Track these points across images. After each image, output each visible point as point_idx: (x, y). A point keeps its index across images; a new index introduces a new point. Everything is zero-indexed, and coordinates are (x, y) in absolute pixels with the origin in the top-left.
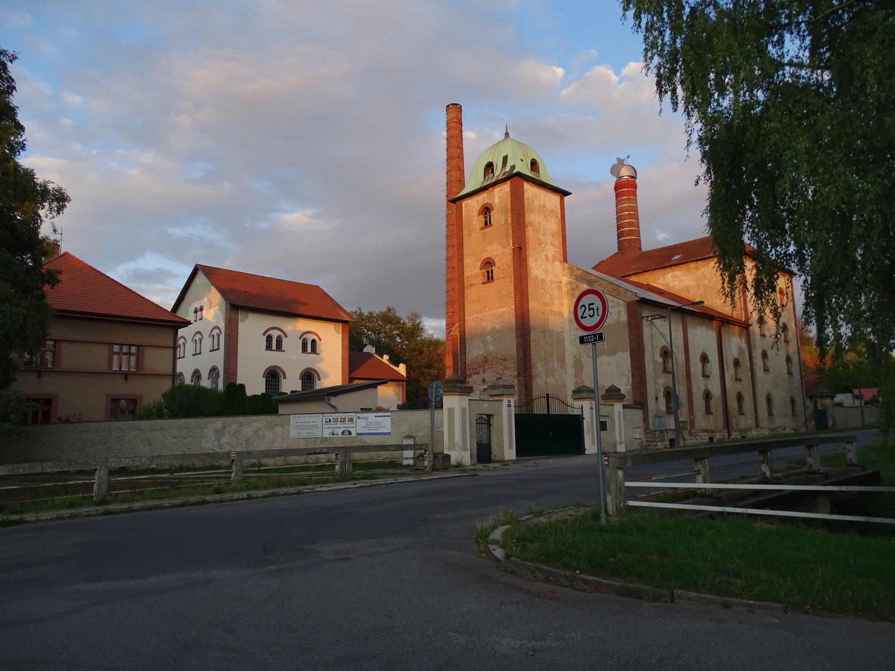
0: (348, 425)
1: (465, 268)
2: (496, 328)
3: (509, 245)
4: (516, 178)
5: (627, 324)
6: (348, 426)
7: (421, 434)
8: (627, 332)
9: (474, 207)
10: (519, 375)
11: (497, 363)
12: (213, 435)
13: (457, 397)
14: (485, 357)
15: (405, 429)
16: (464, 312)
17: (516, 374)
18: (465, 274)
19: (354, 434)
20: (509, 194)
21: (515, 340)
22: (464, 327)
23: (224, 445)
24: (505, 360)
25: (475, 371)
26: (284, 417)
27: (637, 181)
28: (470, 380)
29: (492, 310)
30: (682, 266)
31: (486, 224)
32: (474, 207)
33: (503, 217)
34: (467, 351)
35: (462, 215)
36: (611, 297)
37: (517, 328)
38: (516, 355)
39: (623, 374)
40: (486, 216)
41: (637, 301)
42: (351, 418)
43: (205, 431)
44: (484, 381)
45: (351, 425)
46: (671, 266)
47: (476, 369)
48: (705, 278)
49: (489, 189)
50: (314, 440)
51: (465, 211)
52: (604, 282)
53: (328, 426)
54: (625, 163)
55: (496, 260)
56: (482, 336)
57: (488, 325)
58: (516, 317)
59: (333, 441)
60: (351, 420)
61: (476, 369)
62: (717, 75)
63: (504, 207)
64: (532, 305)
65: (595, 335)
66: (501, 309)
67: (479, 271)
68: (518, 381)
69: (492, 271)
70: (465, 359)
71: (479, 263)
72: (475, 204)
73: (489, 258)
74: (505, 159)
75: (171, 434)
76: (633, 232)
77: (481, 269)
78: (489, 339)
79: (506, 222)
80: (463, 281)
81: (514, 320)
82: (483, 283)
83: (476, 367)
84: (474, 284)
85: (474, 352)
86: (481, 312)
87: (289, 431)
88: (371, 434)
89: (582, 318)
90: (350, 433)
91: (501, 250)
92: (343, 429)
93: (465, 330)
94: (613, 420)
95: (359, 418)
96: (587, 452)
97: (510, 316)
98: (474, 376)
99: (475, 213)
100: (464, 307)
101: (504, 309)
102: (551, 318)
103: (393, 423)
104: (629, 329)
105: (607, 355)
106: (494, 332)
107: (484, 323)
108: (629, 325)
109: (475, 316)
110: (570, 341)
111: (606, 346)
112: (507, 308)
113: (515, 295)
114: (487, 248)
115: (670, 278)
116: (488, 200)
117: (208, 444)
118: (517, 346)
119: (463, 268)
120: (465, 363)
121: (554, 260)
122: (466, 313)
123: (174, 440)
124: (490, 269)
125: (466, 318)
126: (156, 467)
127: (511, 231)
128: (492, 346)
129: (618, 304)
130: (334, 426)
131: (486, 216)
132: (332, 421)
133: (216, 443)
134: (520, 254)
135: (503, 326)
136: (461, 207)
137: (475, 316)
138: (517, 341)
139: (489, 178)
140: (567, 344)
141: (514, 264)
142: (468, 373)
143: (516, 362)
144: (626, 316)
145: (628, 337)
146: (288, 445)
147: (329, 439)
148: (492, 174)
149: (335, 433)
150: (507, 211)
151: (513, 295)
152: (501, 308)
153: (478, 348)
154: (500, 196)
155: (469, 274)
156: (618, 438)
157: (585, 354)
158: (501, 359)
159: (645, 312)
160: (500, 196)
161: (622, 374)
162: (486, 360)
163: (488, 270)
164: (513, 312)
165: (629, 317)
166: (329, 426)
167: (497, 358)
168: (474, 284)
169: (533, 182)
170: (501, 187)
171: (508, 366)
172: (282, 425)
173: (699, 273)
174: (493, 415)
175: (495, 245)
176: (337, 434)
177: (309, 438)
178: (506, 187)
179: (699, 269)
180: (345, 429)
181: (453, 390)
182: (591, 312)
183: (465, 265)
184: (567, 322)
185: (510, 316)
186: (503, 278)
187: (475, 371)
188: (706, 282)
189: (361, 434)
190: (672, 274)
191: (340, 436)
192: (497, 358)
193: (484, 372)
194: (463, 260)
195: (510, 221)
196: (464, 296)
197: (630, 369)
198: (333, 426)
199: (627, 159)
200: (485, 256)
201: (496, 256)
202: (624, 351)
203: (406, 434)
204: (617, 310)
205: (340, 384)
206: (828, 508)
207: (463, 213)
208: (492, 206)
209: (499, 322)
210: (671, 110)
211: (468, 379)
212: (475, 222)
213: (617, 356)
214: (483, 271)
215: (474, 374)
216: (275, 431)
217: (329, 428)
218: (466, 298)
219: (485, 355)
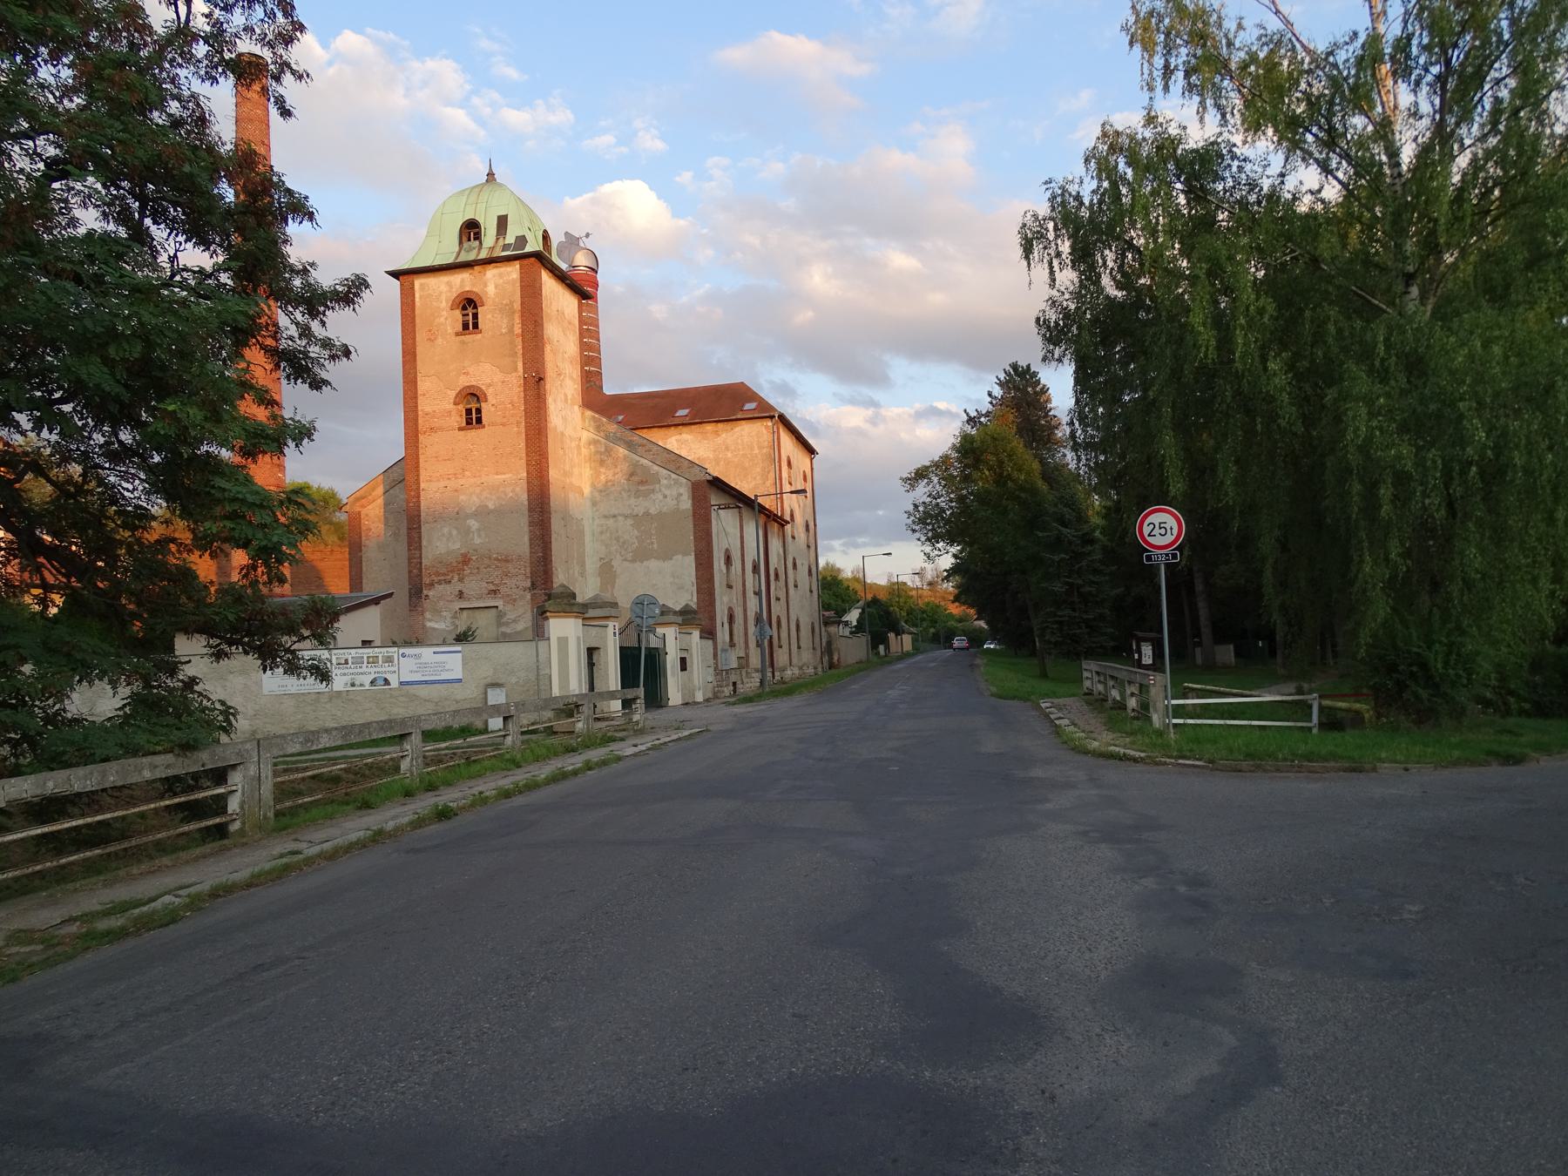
0: (384, 670)
1: (420, 398)
2: (487, 506)
3: (516, 370)
4: (533, 259)
5: (691, 513)
6: (383, 669)
7: (514, 680)
8: (691, 526)
9: (441, 293)
10: (533, 586)
11: (489, 566)
13: (572, 620)
14: (465, 556)
15: (486, 672)
16: (418, 476)
17: (528, 584)
18: (419, 408)
19: (394, 684)
20: (518, 284)
21: (526, 529)
22: (419, 502)
24: (507, 561)
25: (442, 578)
27: (599, 277)
28: (431, 593)
29: (480, 476)
30: (693, 427)
31: (465, 326)
32: (441, 293)
33: (505, 321)
34: (424, 543)
35: (413, 301)
36: (665, 471)
37: (530, 510)
38: (528, 554)
39: (683, 588)
40: (466, 312)
41: (708, 481)
42: (389, 657)
44: (461, 595)
45: (389, 669)
46: (676, 425)
47: (444, 574)
48: (727, 449)
49: (476, 268)
50: (314, 697)
51: (421, 297)
52: (655, 448)
53: (343, 671)
54: (582, 245)
55: (490, 392)
56: (458, 516)
57: (471, 498)
58: (529, 491)
59: (352, 697)
60: (389, 660)
61: (444, 574)
63: (507, 305)
64: (553, 474)
65: (1167, 555)
66: (499, 477)
67: (452, 406)
68: (532, 595)
69: (479, 411)
70: (421, 557)
71: (452, 394)
72: (444, 288)
73: (473, 386)
74: (502, 222)
76: (593, 360)
77: (455, 404)
79: (511, 330)
80: (417, 420)
81: (525, 497)
82: (461, 429)
83: (444, 570)
84: (441, 429)
85: (439, 545)
86: (456, 478)
88: (426, 682)
89: (1149, 535)
90: (387, 682)
91: (498, 377)
92: (372, 677)
93: (419, 507)
94: (691, 655)
95: (404, 655)
96: (671, 703)
97: (518, 489)
98: (440, 588)
99: (444, 304)
100: (418, 467)
101: (503, 477)
102: (572, 496)
103: (465, 663)
104: (694, 521)
105: (657, 558)
106: (482, 513)
107: (462, 497)
108: (694, 516)
109: (442, 484)
110: (593, 535)
111: (655, 546)
112: (510, 475)
113: (527, 455)
114: (471, 370)
115: (675, 443)
116: (473, 285)
118: (531, 540)
119: (416, 398)
120: (421, 563)
121: (573, 404)
122: (421, 478)
124: (474, 406)
125: (422, 485)
127: (520, 347)
128: (479, 536)
129: (676, 482)
130: (356, 671)
131: (466, 312)
132: (350, 662)
134: (539, 389)
135: (502, 505)
136: (413, 288)
137: (442, 484)
138: (531, 531)
139: (470, 250)
140: (588, 538)
141: (525, 403)
142: (426, 580)
143: (528, 565)
144: (690, 502)
145: (692, 533)
146: (257, 707)
147: (344, 695)
148: (477, 242)
149: (357, 683)
150: (514, 312)
151: (524, 455)
152: (497, 474)
153: (448, 539)
154: (498, 284)
155: (428, 409)
156: (696, 682)
157: (618, 556)
158: (497, 559)
159: (715, 499)
160: (498, 284)
161: (681, 588)
162: (466, 560)
163: (469, 406)
164: (524, 484)
165: (694, 505)
166: (346, 671)
167: (490, 558)
168: (441, 429)
169: (551, 271)
170: (502, 270)
171: (512, 571)
173: (719, 440)
174: (598, 648)
175: (487, 366)
176: (361, 685)
177: (303, 694)
178: (513, 272)
179: (719, 435)
180: (377, 675)
181: (568, 609)
182: (1163, 531)
183: (419, 392)
184: (588, 503)
185: (518, 489)
186: (503, 425)
187: (442, 578)
188: (729, 455)
189: (408, 683)
190: (678, 437)
191: (367, 688)
192: (490, 558)
193: (461, 580)
194: (416, 382)
195: (518, 330)
196: (418, 447)
197: (695, 581)
198: (351, 671)
199: (584, 239)
200: (464, 381)
201: (490, 385)
202: (685, 554)
203: (489, 680)
204: (675, 493)
207: (417, 299)
208: (481, 298)
209: (494, 497)
211: (425, 592)
212: (442, 319)
213: (673, 562)
214: (462, 408)
215: (439, 583)
216: (228, 684)
217: (345, 674)
218: (421, 451)
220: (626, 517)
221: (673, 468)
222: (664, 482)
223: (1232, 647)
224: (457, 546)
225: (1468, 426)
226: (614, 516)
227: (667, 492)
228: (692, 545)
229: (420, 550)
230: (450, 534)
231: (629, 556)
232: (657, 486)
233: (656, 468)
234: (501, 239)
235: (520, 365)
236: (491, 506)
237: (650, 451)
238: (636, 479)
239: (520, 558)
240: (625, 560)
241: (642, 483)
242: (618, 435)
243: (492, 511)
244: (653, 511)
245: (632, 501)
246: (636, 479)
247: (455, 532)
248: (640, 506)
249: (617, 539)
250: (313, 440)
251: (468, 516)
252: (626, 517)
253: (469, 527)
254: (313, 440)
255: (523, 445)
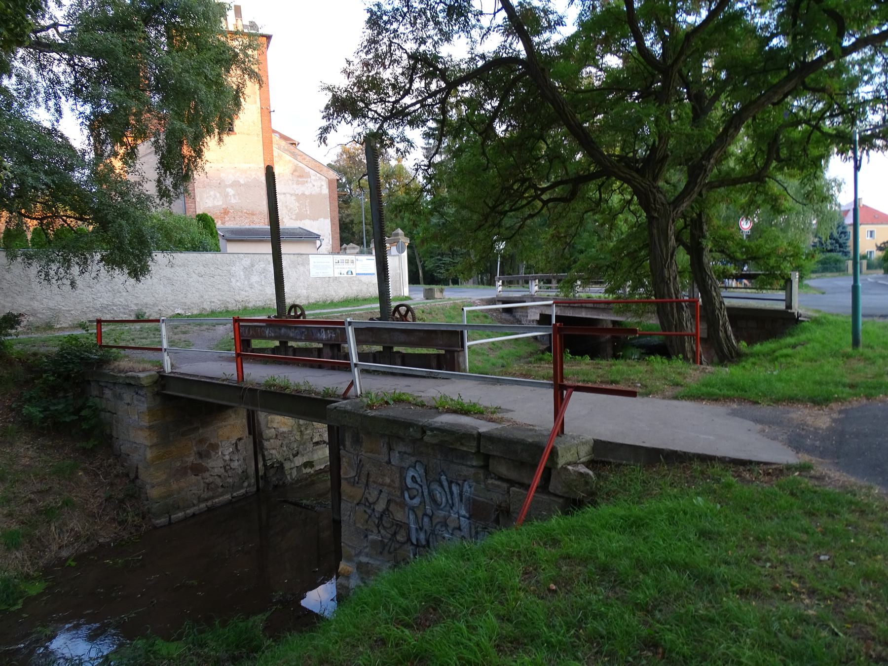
0: (350, 267)
3: (256, 102)
12: (242, 273)
19: (354, 274)
23: (254, 284)
24: (253, 214)
26: (305, 256)
43: (234, 268)
56: (220, 185)
60: (352, 262)
62: (496, 110)
75: (196, 272)
78: (231, 191)
87: (309, 271)
105: (310, 219)
106: (235, 184)
108: (330, 197)
111: (308, 212)
117: (238, 284)
123: (201, 279)
126: (183, 312)
128: (235, 198)
133: (246, 283)
145: (329, 207)
153: (214, 199)
158: (246, 213)
167: (242, 212)
171: (256, 220)
172: (303, 264)
186: (248, 134)
191: (346, 275)
192: (242, 212)
202: (325, 218)
205: (281, 227)
206: (372, 360)
210: (355, 50)
219: (224, 206)
220: (292, 195)
221: (318, 170)
222: (313, 177)
223: (797, 274)
224: (221, 203)
225: (667, 187)
226: (284, 194)
227: (315, 183)
228: (329, 213)
229: (195, 204)
230: (215, 196)
231: (294, 217)
232: (309, 180)
233: (308, 169)
234: (239, 20)
235: (258, 100)
236: (242, 182)
237: (305, 159)
238: (296, 174)
239: (261, 213)
240: (291, 219)
241: (300, 176)
242: (286, 148)
243: (243, 185)
244: (307, 193)
245: (295, 186)
246: (296, 174)
247: (218, 195)
248: (300, 190)
249: (286, 207)
250: (323, 118)
251: (227, 186)
252: (292, 195)
253: (228, 193)
254: (323, 118)
255: (261, 148)
